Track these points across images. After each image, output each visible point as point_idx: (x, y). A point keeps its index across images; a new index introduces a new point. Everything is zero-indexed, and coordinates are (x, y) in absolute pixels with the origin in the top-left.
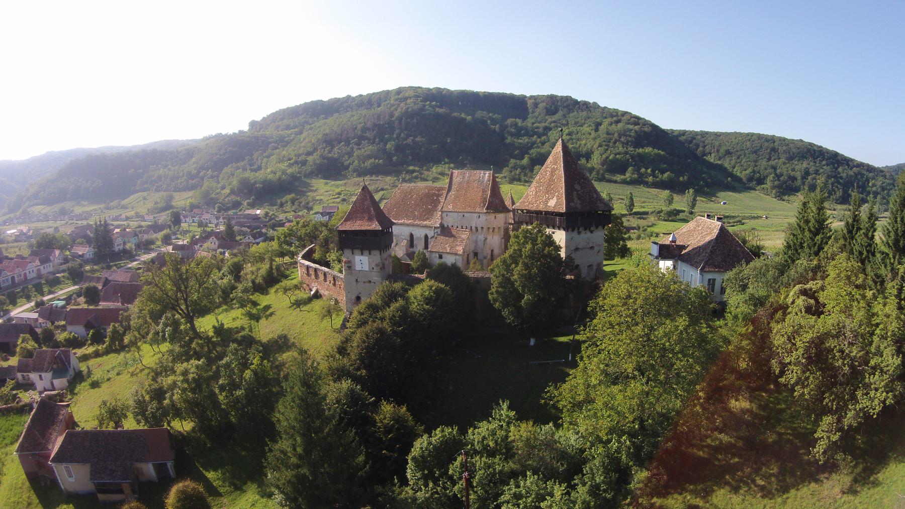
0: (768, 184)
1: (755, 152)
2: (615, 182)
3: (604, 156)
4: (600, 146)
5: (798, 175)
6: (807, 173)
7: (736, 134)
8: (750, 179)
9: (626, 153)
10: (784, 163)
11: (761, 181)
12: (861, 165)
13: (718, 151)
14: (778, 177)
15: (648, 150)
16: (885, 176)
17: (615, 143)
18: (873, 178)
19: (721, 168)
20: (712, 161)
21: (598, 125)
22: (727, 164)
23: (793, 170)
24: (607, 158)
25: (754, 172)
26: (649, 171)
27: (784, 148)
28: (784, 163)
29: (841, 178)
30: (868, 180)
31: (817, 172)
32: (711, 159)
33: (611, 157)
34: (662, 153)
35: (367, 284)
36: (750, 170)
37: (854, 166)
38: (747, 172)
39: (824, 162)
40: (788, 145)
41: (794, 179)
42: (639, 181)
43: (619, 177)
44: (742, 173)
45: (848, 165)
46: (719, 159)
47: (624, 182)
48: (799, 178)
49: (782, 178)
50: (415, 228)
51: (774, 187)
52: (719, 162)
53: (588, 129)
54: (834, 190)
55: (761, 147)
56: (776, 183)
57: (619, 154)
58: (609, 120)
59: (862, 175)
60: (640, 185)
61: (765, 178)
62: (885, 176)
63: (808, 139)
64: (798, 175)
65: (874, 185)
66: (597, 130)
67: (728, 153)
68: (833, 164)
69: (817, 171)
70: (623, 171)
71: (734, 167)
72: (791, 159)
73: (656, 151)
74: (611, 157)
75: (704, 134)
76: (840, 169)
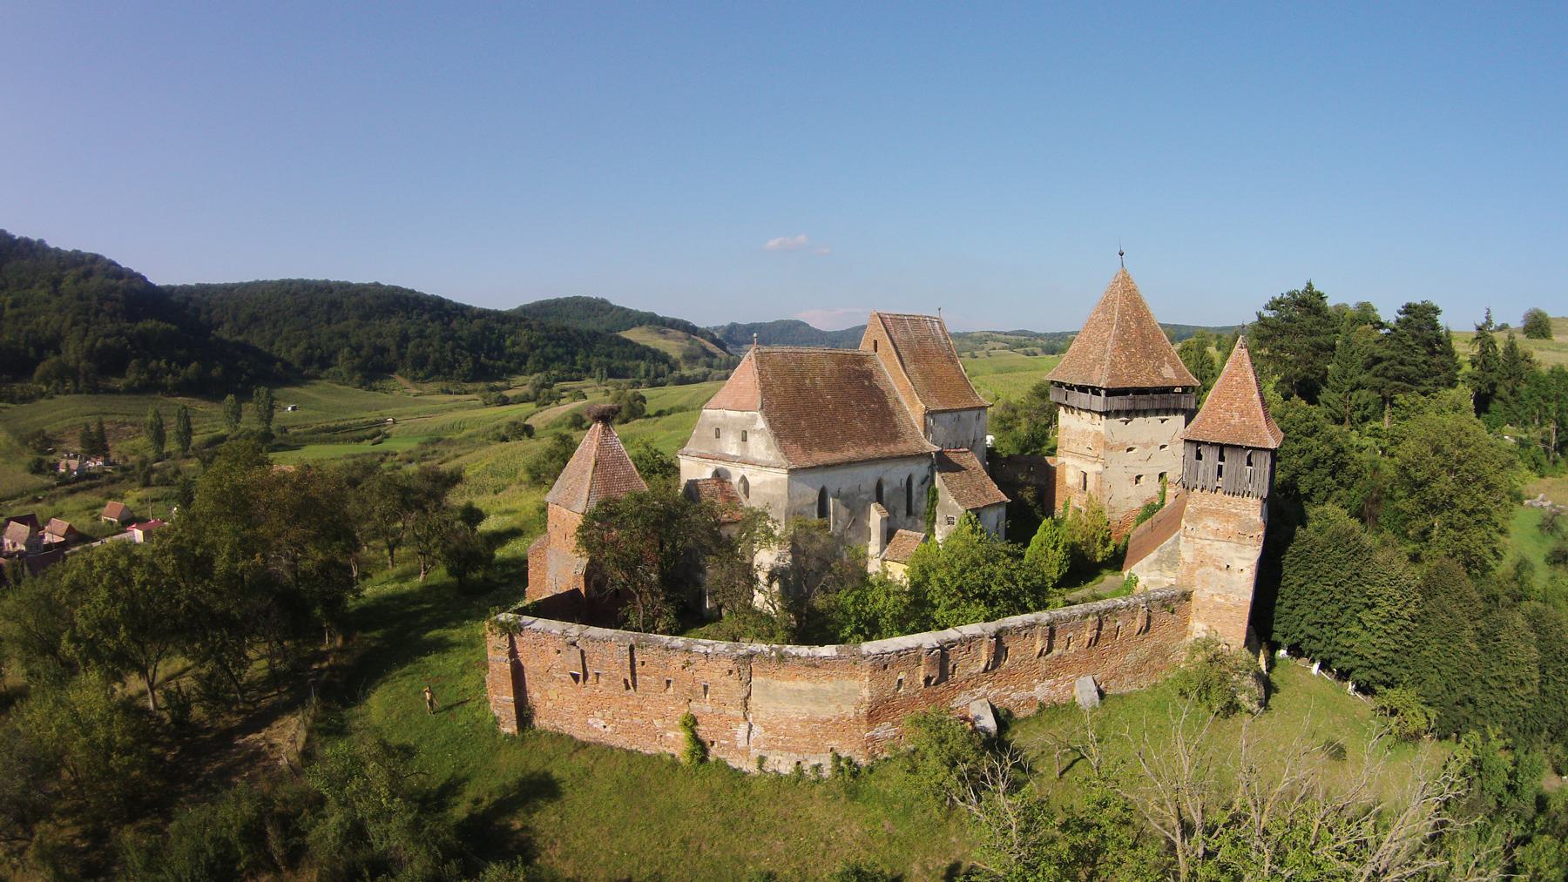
0: (342, 364)
1: (302, 312)
2: (115, 392)
3: (87, 343)
4: (75, 323)
5: (390, 343)
6: (405, 339)
7: (257, 284)
8: (308, 361)
9: (120, 333)
10: (360, 326)
11: (325, 362)
12: (484, 314)
13: (235, 319)
14: (357, 349)
15: (150, 324)
16: (529, 327)
17: (97, 315)
18: (512, 333)
19: (245, 348)
20: (226, 337)
21: (56, 282)
22: (257, 340)
23: (379, 335)
24: (93, 345)
25: (310, 346)
26: (163, 364)
27: (354, 300)
28: (360, 326)
29: (460, 338)
30: (502, 336)
31: (421, 334)
32: (224, 333)
33: (98, 344)
34: (174, 327)
35: (454, 699)
36: (303, 345)
37: (474, 317)
38: (299, 349)
39: (426, 317)
40: (357, 294)
41: (383, 350)
42: (149, 387)
43: (118, 383)
44: (294, 355)
45: (463, 316)
46: (240, 332)
47: (130, 390)
48: (393, 348)
49: (363, 353)
50: (888, 466)
51: (353, 370)
52: (240, 338)
53: (42, 293)
54: (457, 361)
55: (311, 302)
56: (357, 361)
57: (107, 336)
58: (73, 271)
59: (492, 330)
60: (155, 392)
61: (333, 354)
62: (529, 327)
63: (388, 280)
64: (390, 343)
65: (514, 344)
66: (57, 292)
67: (254, 319)
68: (440, 317)
69: (422, 331)
70: (120, 370)
71: (272, 344)
72: (367, 317)
73: (163, 325)
74: (98, 344)
75: (204, 289)
76: (455, 324)
